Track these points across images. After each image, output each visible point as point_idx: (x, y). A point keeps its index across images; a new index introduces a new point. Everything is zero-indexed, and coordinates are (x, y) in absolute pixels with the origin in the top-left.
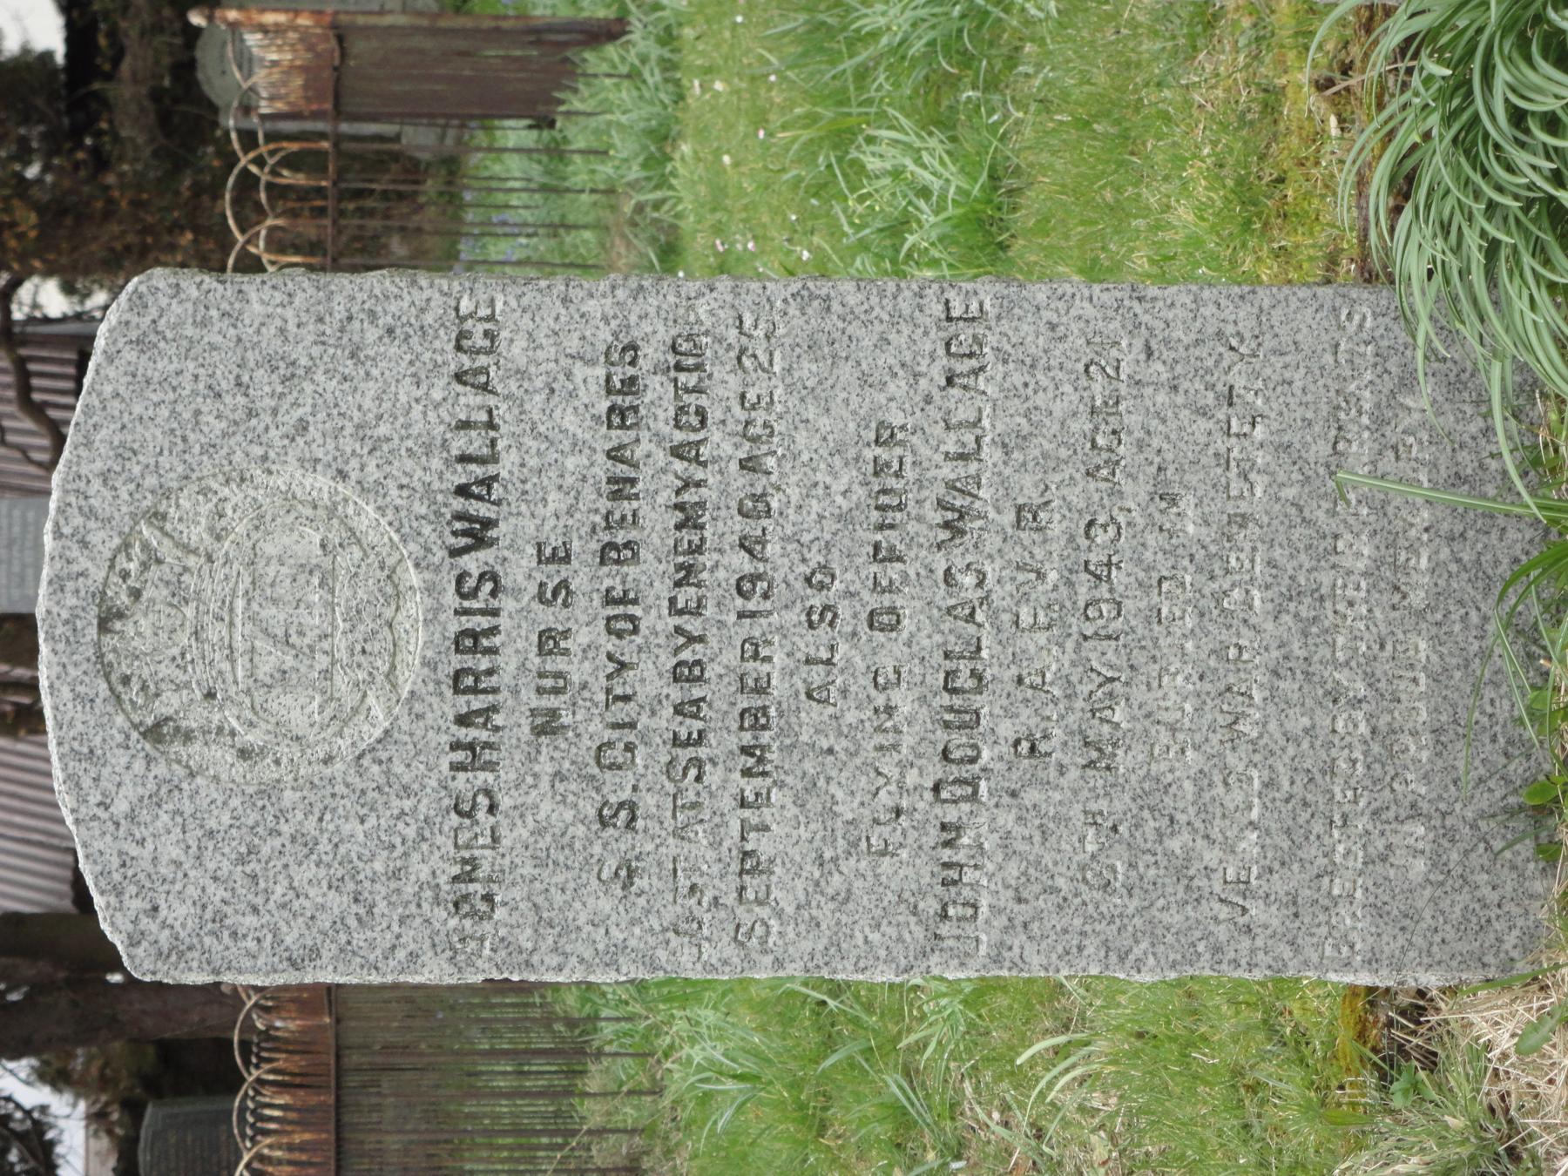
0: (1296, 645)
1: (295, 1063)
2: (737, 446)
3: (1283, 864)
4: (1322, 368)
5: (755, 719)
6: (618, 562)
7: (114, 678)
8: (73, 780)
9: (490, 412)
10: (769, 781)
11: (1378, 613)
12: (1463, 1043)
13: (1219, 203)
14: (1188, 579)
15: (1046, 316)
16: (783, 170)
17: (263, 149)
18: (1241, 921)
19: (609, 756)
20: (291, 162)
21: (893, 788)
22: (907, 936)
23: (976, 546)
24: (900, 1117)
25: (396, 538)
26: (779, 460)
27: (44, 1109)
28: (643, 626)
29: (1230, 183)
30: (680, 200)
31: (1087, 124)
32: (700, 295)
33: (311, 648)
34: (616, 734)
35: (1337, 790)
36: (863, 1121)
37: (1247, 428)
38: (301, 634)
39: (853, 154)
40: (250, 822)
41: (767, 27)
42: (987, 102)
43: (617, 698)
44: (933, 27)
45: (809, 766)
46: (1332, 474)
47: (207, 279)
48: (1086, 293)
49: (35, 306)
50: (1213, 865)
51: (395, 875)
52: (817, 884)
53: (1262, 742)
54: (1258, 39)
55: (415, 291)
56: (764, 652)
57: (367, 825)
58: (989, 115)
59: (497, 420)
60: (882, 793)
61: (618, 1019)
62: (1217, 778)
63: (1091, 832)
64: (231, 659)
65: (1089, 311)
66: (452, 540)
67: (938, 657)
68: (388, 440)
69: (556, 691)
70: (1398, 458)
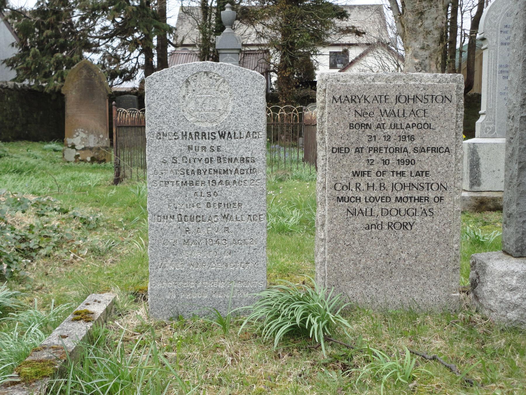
5: (191, 183)
8: (179, 67)
19: (185, 159)
27: (136, 79)
36: (131, 213)
51: (164, 122)
62: (183, 262)
65: (262, 239)
67: (203, 214)
69: (196, 149)
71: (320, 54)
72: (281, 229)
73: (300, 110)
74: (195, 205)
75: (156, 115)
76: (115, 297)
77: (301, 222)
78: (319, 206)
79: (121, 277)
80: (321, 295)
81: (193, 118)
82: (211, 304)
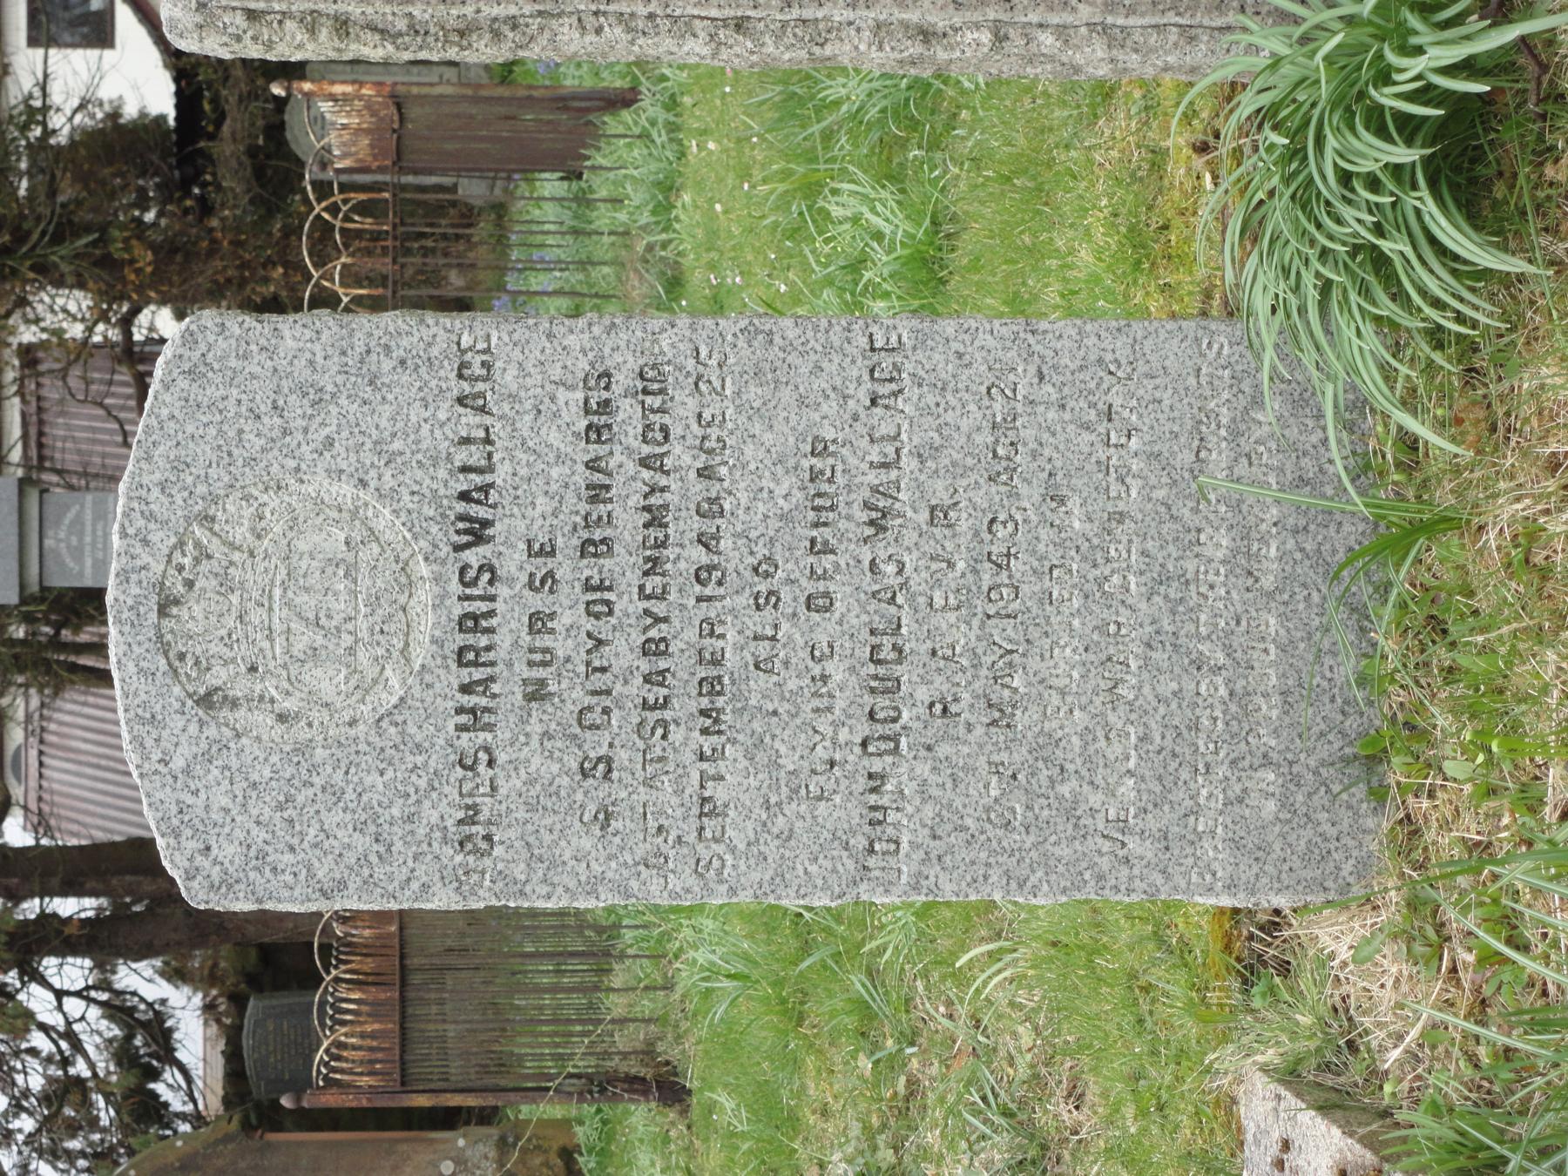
0: (1165, 622)
1: (369, 964)
2: (695, 458)
3: (1155, 805)
4: (1187, 389)
5: (711, 686)
6: (595, 555)
7: (171, 654)
8: (138, 741)
9: (487, 430)
10: (724, 738)
11: (1234, 594)
12: (1311, 953)
13: (1114, 246)
14: (1075, 567)
15: (974, 339)
16: (763, 217)
17: (338, 198)
18: (1121, 853)
19: (589, 718)
20: (363, 209)
21: (828, 743)
22: (840, 868)
23: (896, 540)
24: (865, 1011)
25: (408, 536)
26: (730, 469)
27: (163, 1002)
28: (617, 609)
29: (1123, 230)
30: (682, 241)
31: (1009, 179)
32: (664, 330)
33: (338, 629)
34: (594, 700)
35: (1201, 743)
36: (833, 1014)
37: (1123, 440)
38: (329, 617)
39: (820, 203)
40: (288, 776)
41: (750, 97)
42: (930, 159)
43: (596, 670)
44: (885, 97)
45: (757, 726)
46: (1195, 477)
47: (247, 318)
48: (988, 327)
49: (151, 329)
50: (1097, 806)
51: (410, 819)
52: (764, 824)
53: (1137, 704)
54: (1146, 108)
55: (423, 328)
56: (719, 630)
57: (386, 777)
58: (931, 171)
59: (493, 437)
60: (819, 748)
61: (637, 927)
62: (1100, 734)
63: (995, 779)
64: (270, 638)
65: (990, 342)
66: (456, 538)
67: (865, 634)
68: (402, 454)
69: (544, 664)
70: (1250, 464)
71: (45, 95)
72: (924, 274)
73: (323, 189)
74: (817, 671)
75: (374, 859)
76: (1264, 1069)
77: (890, 177)
78: (828, 50)
79: (1154, 1053)
80: (1274, 43)
81: (388, 672)
82: (1308, 598)
